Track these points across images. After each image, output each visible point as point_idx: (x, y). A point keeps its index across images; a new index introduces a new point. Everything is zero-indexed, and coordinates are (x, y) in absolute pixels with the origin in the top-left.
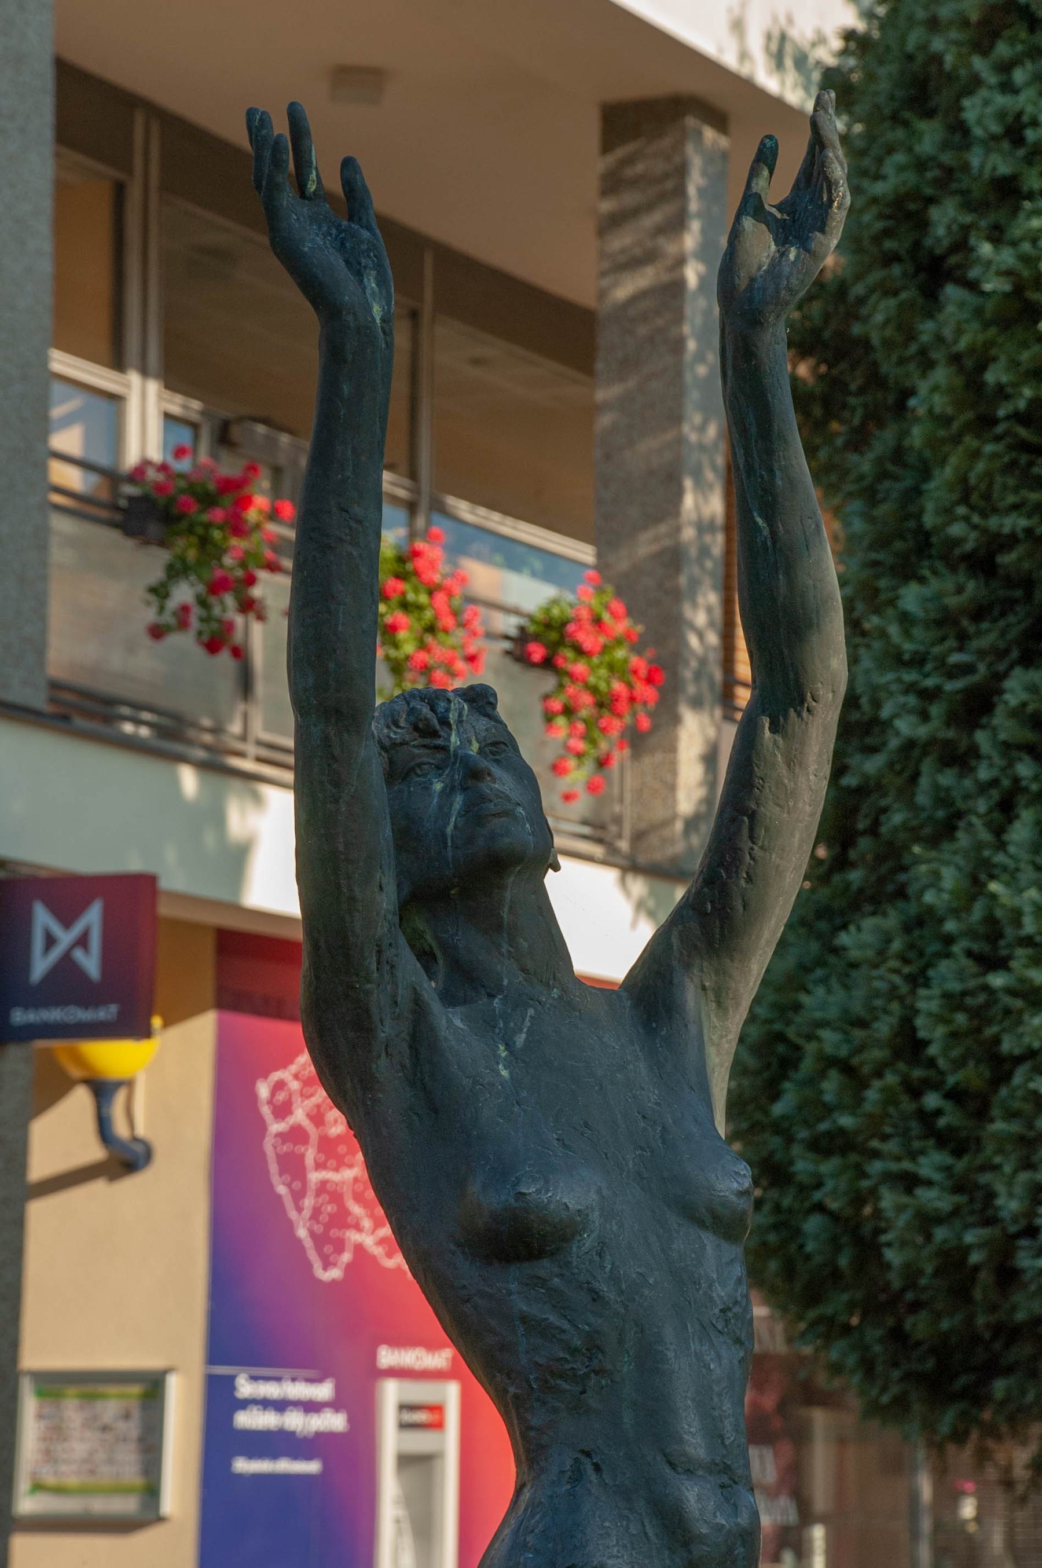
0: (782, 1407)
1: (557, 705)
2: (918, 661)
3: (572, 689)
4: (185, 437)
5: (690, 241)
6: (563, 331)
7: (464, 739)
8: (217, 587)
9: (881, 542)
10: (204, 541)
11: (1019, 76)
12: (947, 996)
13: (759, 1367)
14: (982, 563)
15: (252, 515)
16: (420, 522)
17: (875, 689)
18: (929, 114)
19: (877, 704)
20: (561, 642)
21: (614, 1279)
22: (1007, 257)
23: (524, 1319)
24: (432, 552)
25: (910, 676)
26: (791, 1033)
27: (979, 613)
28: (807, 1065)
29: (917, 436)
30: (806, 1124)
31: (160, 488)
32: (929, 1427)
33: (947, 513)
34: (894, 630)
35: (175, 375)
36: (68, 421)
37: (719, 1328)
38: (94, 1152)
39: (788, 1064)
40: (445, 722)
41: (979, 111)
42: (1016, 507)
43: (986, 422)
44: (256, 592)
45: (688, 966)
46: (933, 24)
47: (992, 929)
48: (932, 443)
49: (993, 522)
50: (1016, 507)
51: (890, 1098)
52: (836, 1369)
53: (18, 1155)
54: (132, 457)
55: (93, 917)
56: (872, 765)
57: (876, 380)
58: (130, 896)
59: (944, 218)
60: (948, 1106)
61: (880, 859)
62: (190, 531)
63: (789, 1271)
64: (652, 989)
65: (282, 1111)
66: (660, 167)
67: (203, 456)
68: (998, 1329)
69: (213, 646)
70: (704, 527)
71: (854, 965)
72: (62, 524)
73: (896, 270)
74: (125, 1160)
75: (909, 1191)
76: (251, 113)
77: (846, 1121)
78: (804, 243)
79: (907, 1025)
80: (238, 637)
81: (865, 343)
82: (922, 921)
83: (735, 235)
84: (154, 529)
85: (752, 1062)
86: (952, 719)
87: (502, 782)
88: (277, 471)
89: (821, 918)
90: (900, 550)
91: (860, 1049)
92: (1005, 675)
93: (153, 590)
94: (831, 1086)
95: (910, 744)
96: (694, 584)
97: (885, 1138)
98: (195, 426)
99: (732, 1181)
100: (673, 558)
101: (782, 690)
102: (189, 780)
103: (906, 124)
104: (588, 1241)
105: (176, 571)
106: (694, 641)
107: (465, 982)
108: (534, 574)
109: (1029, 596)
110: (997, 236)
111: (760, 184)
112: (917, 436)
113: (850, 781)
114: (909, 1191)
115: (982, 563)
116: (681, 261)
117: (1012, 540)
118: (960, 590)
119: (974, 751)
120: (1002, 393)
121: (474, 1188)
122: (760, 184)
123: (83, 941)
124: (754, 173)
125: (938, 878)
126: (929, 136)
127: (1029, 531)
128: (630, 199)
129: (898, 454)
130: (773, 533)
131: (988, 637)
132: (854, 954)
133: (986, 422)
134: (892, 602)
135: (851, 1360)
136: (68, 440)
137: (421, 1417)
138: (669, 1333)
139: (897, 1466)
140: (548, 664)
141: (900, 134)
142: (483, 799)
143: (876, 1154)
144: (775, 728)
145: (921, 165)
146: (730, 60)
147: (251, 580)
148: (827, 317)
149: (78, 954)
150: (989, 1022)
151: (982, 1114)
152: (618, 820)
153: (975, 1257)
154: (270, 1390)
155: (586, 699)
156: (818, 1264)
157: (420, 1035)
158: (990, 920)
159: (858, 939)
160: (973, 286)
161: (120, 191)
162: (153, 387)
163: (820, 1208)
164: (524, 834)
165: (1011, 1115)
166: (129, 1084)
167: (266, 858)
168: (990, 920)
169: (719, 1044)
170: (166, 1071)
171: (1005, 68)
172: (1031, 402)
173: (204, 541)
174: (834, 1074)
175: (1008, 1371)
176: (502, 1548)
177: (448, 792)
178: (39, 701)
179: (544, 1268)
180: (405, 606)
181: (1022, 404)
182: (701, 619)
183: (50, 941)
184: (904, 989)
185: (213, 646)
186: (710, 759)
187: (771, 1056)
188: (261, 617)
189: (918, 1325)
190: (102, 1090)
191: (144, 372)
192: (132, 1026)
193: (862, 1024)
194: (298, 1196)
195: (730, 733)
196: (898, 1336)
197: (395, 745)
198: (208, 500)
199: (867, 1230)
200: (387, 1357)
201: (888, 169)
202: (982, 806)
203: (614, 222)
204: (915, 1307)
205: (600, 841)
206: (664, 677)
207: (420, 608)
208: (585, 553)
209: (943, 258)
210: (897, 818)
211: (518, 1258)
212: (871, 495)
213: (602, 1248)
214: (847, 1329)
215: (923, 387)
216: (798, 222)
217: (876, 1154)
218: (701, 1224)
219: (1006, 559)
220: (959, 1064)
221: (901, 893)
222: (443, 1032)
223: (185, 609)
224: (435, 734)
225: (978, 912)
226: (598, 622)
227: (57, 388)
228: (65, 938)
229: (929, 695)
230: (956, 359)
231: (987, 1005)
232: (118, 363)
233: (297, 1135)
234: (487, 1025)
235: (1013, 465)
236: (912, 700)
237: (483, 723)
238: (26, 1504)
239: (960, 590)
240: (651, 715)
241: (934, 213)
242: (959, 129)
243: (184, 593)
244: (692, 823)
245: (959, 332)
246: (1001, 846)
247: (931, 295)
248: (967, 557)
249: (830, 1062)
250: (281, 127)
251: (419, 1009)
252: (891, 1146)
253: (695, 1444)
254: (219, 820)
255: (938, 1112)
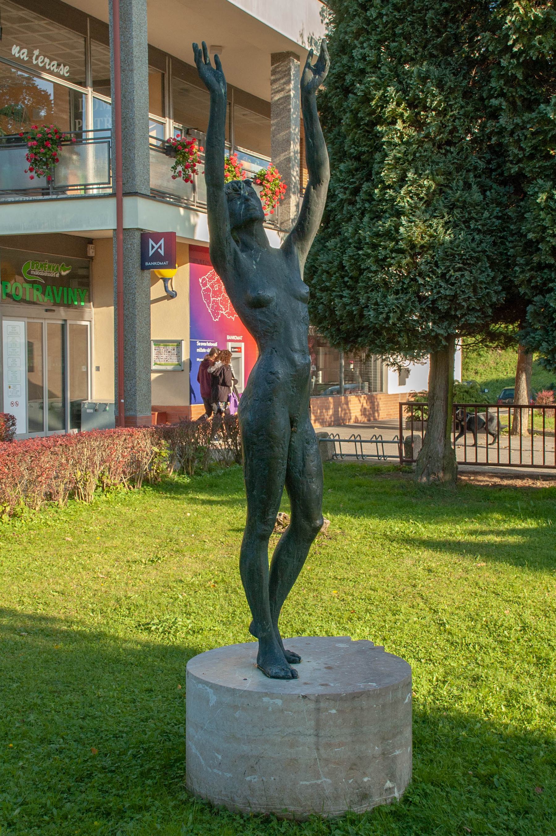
0: (313, 347)
1: (263, 193)
2: (343, 181)
3: (267, 190)
4: (179, 133)
5: (292, 86)
6: (263, 107)
7: (244, 192)
8: (187, 167)
9: (335, 154)
10: (184, 156)
11: (365, 45)
12: (350, 256)
13: (309, 338)
14: (357, 158)
15: (194, 150)
16: (232, 152)
17: (334, 187)
18: (345, 54)
19: (334, 191)
20: (264, 179)
21: (279, 311)
22: (363, 87)
23: (260, 320)
24: (235, 158)
25: (342, 184)
26: (316, 265)
27: (357, 170)
28: (319, 272)
29: (343, 129)
30: (319, 285)
31: (174, 144)
32: (345, 349)
33: (350, 147)
34: (338, 174)
35: (177, 119)
36: (153, 129)
37: (302, 330)
38: (165, 294)
39: (315, 272)
40: (240, 188)
41: (356, 53)
42: (364, 145)
43: (358, 126)
44: (196, 168)
45: (295, 243)
46: (346, 33)
47: (359, 241)
48: (347, 131)
49: (360, 148)
50: (364, 145)
51: (337, 279)
52: (325, 337)
53: (148, 295)
54: (167, 138)
55: (162, 241)
56: (333, 205)
57: (334, 116)
58: (170, 237)
59: (349, 78)
60: (350, 280)
61: (335, 226)
62: (181, 154)
63: (315, 317)
64: (287, 249)
65: (205, 285)
66: (285, 69)
67: (183, 137)
68: (359, 328)
69: (186, 181)
70: (295, 153)
71: (329, 250)
72: (152, 153)
73: (338, 90)
74: (171, 295)
75: (341, 299)
76: (193, 44)
77: (328, 284)
78: (319, 74)
79: (341, 263)
80: (192, 178)
81: (331, 108)
82: (345, 239)
83: (304, 72)
84: (173, 153)
85: (307, 272)
86: (351, 194)
87: (253, 202)
88: (200, 140)
89: (321, 240)
90: (338, 156)
91: (330, 268)
92: (362, 184)
93: (172, 168)
94: (324, 276)
95: (342, 200)
96: (293, 165)
97: (336, 287)
98: (181, 130)
99: (305, 290)
100: (289, 160)
101: (316, 180)
102: (182, 211)
103: (340, 56)
104: (274, 303)
105: (178, 163)
106: (293, 178)
107: (246, 247)
108: (257, 164)
109: (368, 166)
110: (360, 82)
111: (310, 60)
112: (343, 129)
113: (329, 208)
114: (341, 299)
115: (357, 158)
116: (290, 91)
117: (364, 153)
118: (353, 165)
119: (356, 201)
120: (362, 119)
121: (249, 292)
122: (310, 60)
123: (160, 247)
124: (308, 58)
125: (348, 230)
126: (345, 59)
127: (368, 151)
128: (278, 76)
129: (339, 134)
130: (313, 143)
131: (359, 175)
132: (330, 247)
133: (358, 126)
134: (338, 168)
135: (329, 335)
136: (153, 133)
137: (236, 350)
138: (291, 323)
139: (337, 359)
140: (261, 184)
141: (339, 59)
142: (249, 206)
143: (334, 291)
144: (314, 189)
145: (343, 66)
146: (300, 43)
147: (195, 165)
148: (323, 102)
149: (159, 250)
150: (359, 262)
151: (357, 282)
152: (277, 220)
153: (355, 313)
154: (203, 344)
155: (270, 192)
156: (322, 316)
157: (236, 259)
158: (359, 239)
159: (330, 244)
160: (355, 94)
161: (163, 75)
162: (172, 121)
163: (322, 303)
164: (258, 213)
165: (363, 282)
166: (172, 279)
167: (201, 230)
168: (359, 239)
169: (302, 261)
170: (180, 275)
171: (362, 43)
172: (368, 121)
173: (184, 156)
174: (325, 274)
175: (362, 336)
176: (256, 368)
177: (241, 204)
178: (149, 194)
179: (264, 309)
180: (229, 171)
181: (366, 121)
182: (295, 174)
183: (153, 247)
184: (340, 255)
185: (186, 181)
186: (297, 206)
187: (312, 270)
188: (197, 174)
189: (343, 327)
190: (165, 280)
191: (169, 118)
192: (172, 266)
193: (331, 263)
194: (208, 303)
195: (302, 199)
196: (338, 329)
197: (229, 193)
198: (185, 147)
199: (332, 308)
200: (229, 337)
201: (336, 67)
202: (357, 214)
203: (274, 82)
204: (342, 323)
205: (273, 225)
206: (287, 188)
207: (232, 171)
208: (269, 159)
209: (348, 88)
210: (339, 217)
211: (259, 308)
212: (333, 143)
213: (277, 305)
214: (327, 329)
215: (344, 118)
216: (318, 69)
217: (334, 291)
218: (298, 299)
219: (363, 157)
220: (352, 271)
221: (340, 234)
222: (241, 258)
223: (180, 172)
224: (238, 191)
225: (356, 237)
226: (272, 174)
227: (150, 122)
228: (156, 247)
229: (346, 189)
230: (351, 111)
231: (359, 258)
232: (164, 116)
233: (208, 290)
234: (251, 256)
235: (365, 135)
236: (342, 190)
237: (249, 188)
238: (153, 367)
239: (353, 165)
240: (284, 196)
241: (346, 77)
242: (352, 57)
243: (180, 168)
244: (293, 220)
245: (352, 105)
246: (362, 222)
247: (346, 96)
248: (353, 157)
249: (324, 271)
250: (200, 47)
251: (235, 252)
252: (338, 289)
253: (297, 346)
254: (189, 220)
255: (348, 282)
